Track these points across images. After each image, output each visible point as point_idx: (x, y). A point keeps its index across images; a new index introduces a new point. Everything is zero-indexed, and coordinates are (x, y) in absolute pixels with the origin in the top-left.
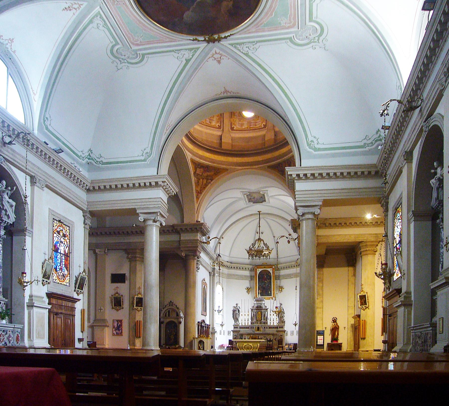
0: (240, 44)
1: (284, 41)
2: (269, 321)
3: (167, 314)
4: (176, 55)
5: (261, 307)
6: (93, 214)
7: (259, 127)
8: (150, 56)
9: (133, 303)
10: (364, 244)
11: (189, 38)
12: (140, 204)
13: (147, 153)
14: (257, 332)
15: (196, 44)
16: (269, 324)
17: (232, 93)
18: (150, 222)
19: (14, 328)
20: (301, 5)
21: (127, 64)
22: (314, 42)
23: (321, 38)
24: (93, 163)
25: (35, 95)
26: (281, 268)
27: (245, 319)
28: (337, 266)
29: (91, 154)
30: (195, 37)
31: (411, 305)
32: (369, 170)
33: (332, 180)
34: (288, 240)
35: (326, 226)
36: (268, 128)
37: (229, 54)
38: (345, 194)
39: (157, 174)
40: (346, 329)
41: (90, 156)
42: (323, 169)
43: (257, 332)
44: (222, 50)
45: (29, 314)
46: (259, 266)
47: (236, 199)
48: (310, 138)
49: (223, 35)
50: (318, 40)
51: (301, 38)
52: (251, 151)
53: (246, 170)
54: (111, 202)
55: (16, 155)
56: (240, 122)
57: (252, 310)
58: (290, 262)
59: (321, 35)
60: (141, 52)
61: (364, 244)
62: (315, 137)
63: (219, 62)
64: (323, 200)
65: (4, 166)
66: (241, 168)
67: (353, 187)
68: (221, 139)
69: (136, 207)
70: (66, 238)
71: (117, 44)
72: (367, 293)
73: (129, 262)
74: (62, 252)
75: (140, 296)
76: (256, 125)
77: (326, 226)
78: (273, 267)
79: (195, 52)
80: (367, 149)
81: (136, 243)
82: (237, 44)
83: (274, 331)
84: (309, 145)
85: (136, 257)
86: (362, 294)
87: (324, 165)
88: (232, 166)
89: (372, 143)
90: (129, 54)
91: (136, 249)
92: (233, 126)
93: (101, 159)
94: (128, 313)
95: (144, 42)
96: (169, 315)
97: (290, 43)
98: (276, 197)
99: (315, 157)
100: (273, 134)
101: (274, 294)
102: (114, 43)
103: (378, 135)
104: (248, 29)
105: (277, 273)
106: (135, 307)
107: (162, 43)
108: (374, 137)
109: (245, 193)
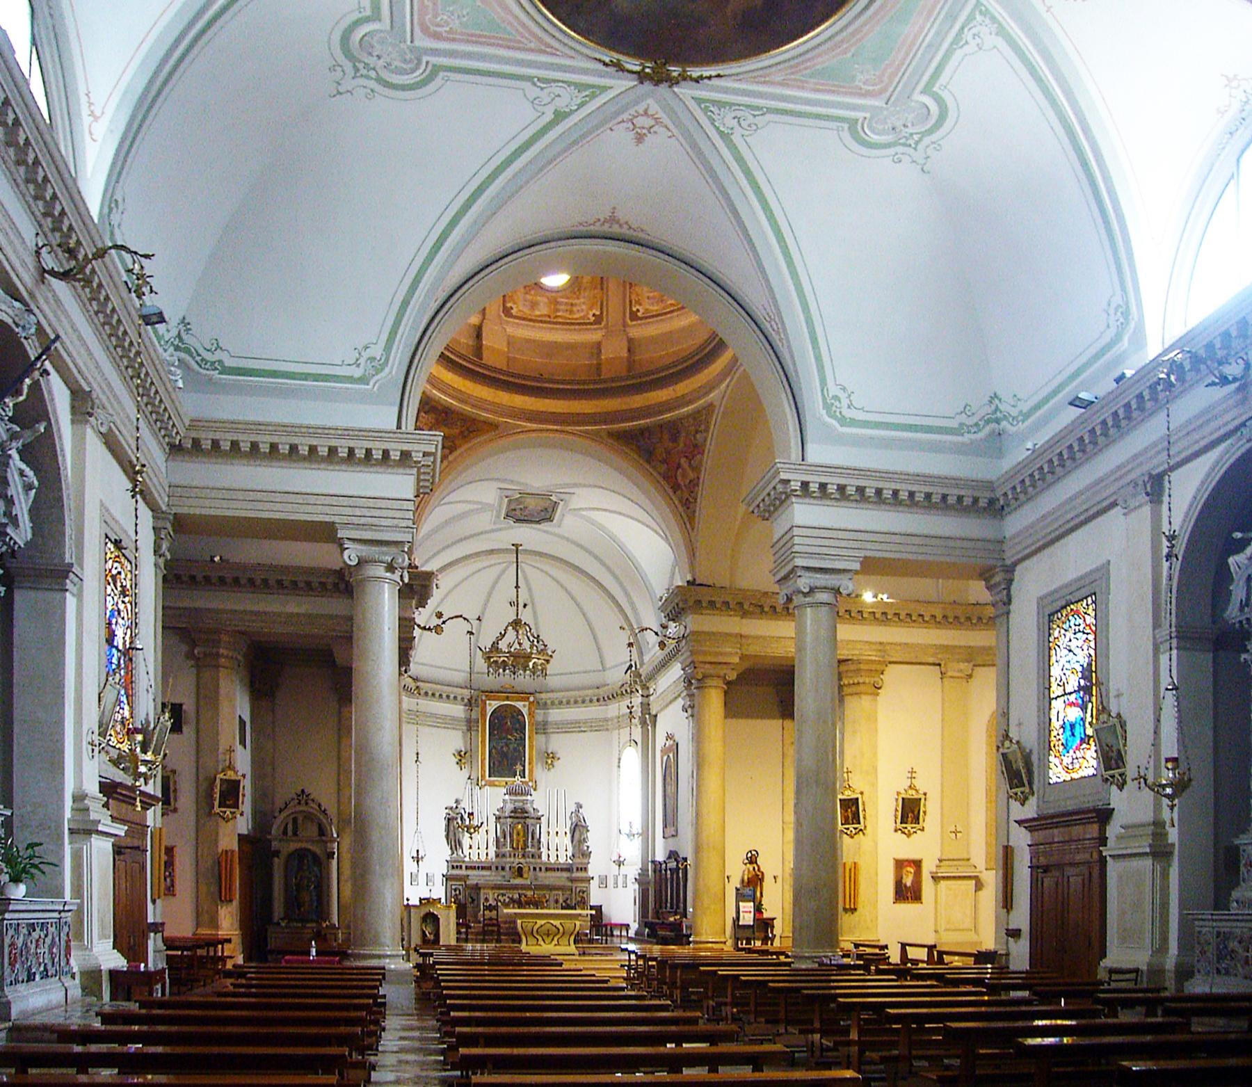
0: (720, 104)
1: (833, 125)
2: (544, 850)
3: (290, 827)
4: (533, 92)
5: (524, 811)
6: (182, 524)
7: (582, 318)
8: (452, 76)
9: (210, 796)
10: (852, 667)
11: (598, 56)
12: (349, 511)
13: (372, 359)
14: (518, 881)
15: (612, 77)
16: (544, 858)
17: (625, 226)
18: (380, 571)
19: (60, 912)
20: (929, 46)
21: (372, 84)
22: (905, 145)
23: (927, 140)
24: (209, 370)
25: (96, 119)
26: (553, 703)
27: (480, 846)
28: (762, 717)
29: (183, 334)
30: (616, 56)
31: (1170, 854)
32: (976, 494)
33: (883, 507)
34: (659, 639)
35: (762, 612)
36: (606, 327)
37: (678, 123)
38: (914, 549)
39: (399, 427)
40: (779, 880)
41: (181, 340)
42: (868, 477)
43: (518, 881)
44: (671, 112)
45: (77, 857)
46: (491, 693)
47: (467, 507)
48: (833, 390)
49: (695, 72)
50: (917, 143)
51: (880, 127)
52: (563, 382)
53: (545, 434)
54: (252, 496)
55: (63, 318)
56: (528, 297)
57: (498, 818)
58: (578, 689)
59: (930, 131)
60: (434, 60)
61: (852, 667)
62: (844, 389)
63: (640, 138)
64: (865, 557)
65: (28, 348)
66: (535, 426)
67: (940, 532)
68: (479, 336)
69: (336, 519)
70: (127, 600)
71: (376, 16)
72: (862, 793)
73: (194, 670)
74: (121, 647)
75: (231, 775)
76: (571, 312)
77: (762, 612)
78: (532, 699)
79: (593, 96)
80: (967, 438)
81: (217, 611)
82: (714, 102)
83: (560, 878)
84: (827, 407)
85: (218, 655)
86: (848, 794)
87: (898, 468)
88: (510, 417)
89: (976, 425)
90: (394, 55)
91: (217, 631)
92: (509, 305)
93: (219, 355)
94: (192, 824)
95: (462, 34)
96: (295, 834)
97: (846, 135)
98: (595, 515)
99: (841, 440)
100: (625, 345)
101: (531, 771)
102: (368, 13)
103: (993, 407)
104: (768, 71)
105: (540, 715)
106: (217, 809)
107: (851, 94)
108: (983, 412)
109: (509, 493)
